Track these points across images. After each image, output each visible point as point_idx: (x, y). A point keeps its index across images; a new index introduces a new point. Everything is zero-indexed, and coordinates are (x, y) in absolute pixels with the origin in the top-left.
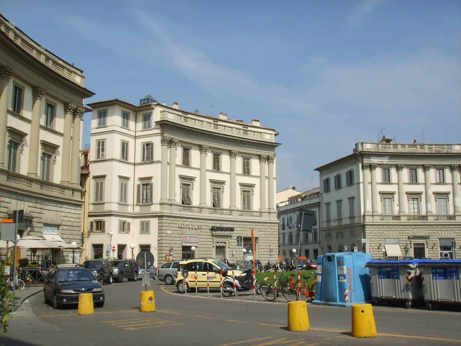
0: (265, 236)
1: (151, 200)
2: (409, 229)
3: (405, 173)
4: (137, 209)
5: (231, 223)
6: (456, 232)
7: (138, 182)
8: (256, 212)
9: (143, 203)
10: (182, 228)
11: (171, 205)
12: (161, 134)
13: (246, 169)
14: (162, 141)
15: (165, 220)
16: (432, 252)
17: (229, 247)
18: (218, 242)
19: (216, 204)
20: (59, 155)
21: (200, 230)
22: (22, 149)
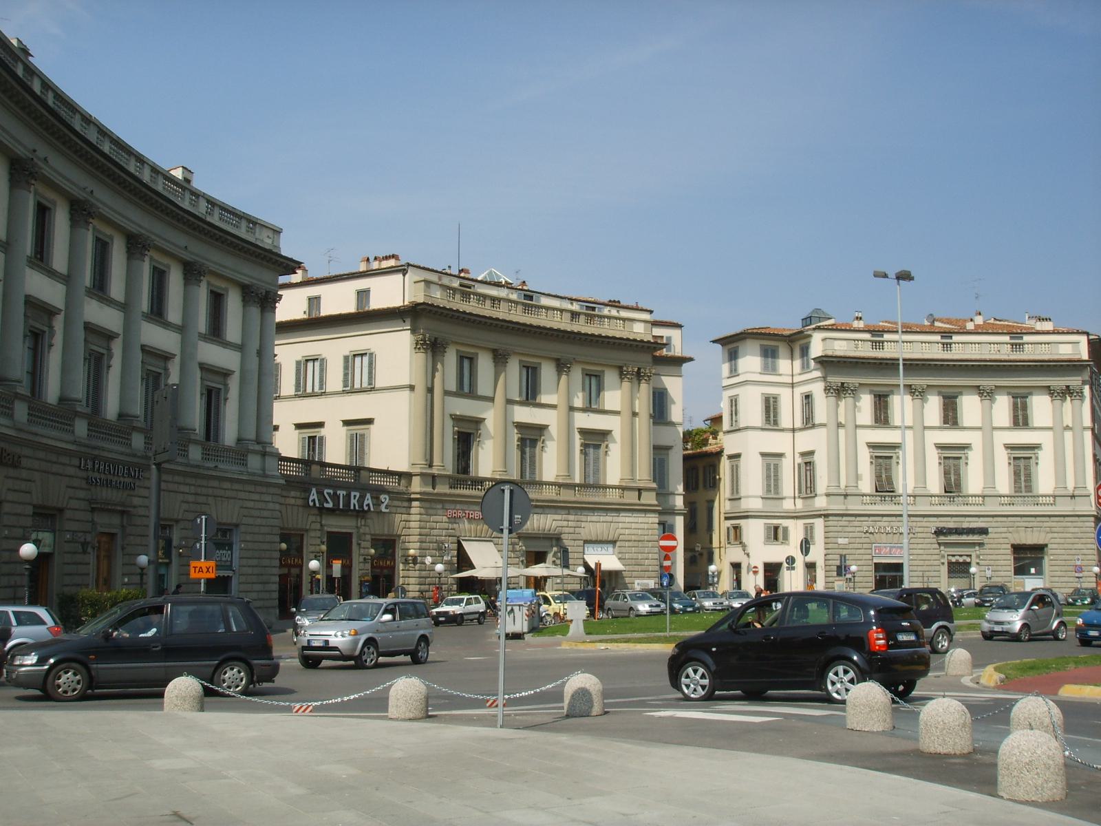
0: (1062, 541)
4: (800, 504)
5: (982, 519)
7: (799, 460)
9: (807, 493)
10: (872, 533)
12: (823, 377)
13: (1020, 417)
14: (825, 390)
18: (953, 556)
19: (953, 487)
20: (615, 442)
22: (542, 445)
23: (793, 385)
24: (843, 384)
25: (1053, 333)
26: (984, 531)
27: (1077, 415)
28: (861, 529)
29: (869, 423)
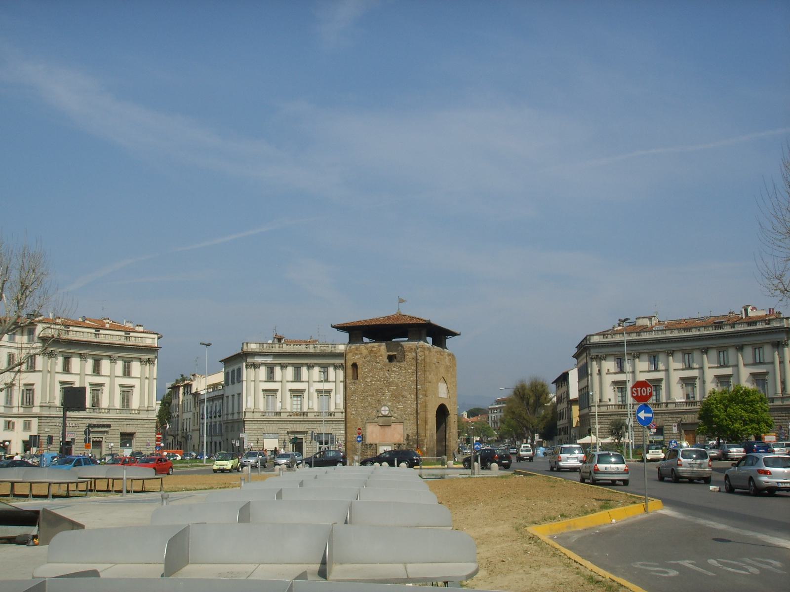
1: (33, 404)
2: (288, 425)
3: (290, 371)
4: (21, 410)
6: (334, 427)
8: (104, 409)
11: (50, 407)
13: (127, 372)
15: (43, 420)
16: (310, 446)
17: (105, 442)
18: (95, 438)
21: (77, 427)
23: (22, 349)
25: (143, 332)
26: (109, 426)
27: (151, 372)
28: (55, 424)
29: (61, 371)
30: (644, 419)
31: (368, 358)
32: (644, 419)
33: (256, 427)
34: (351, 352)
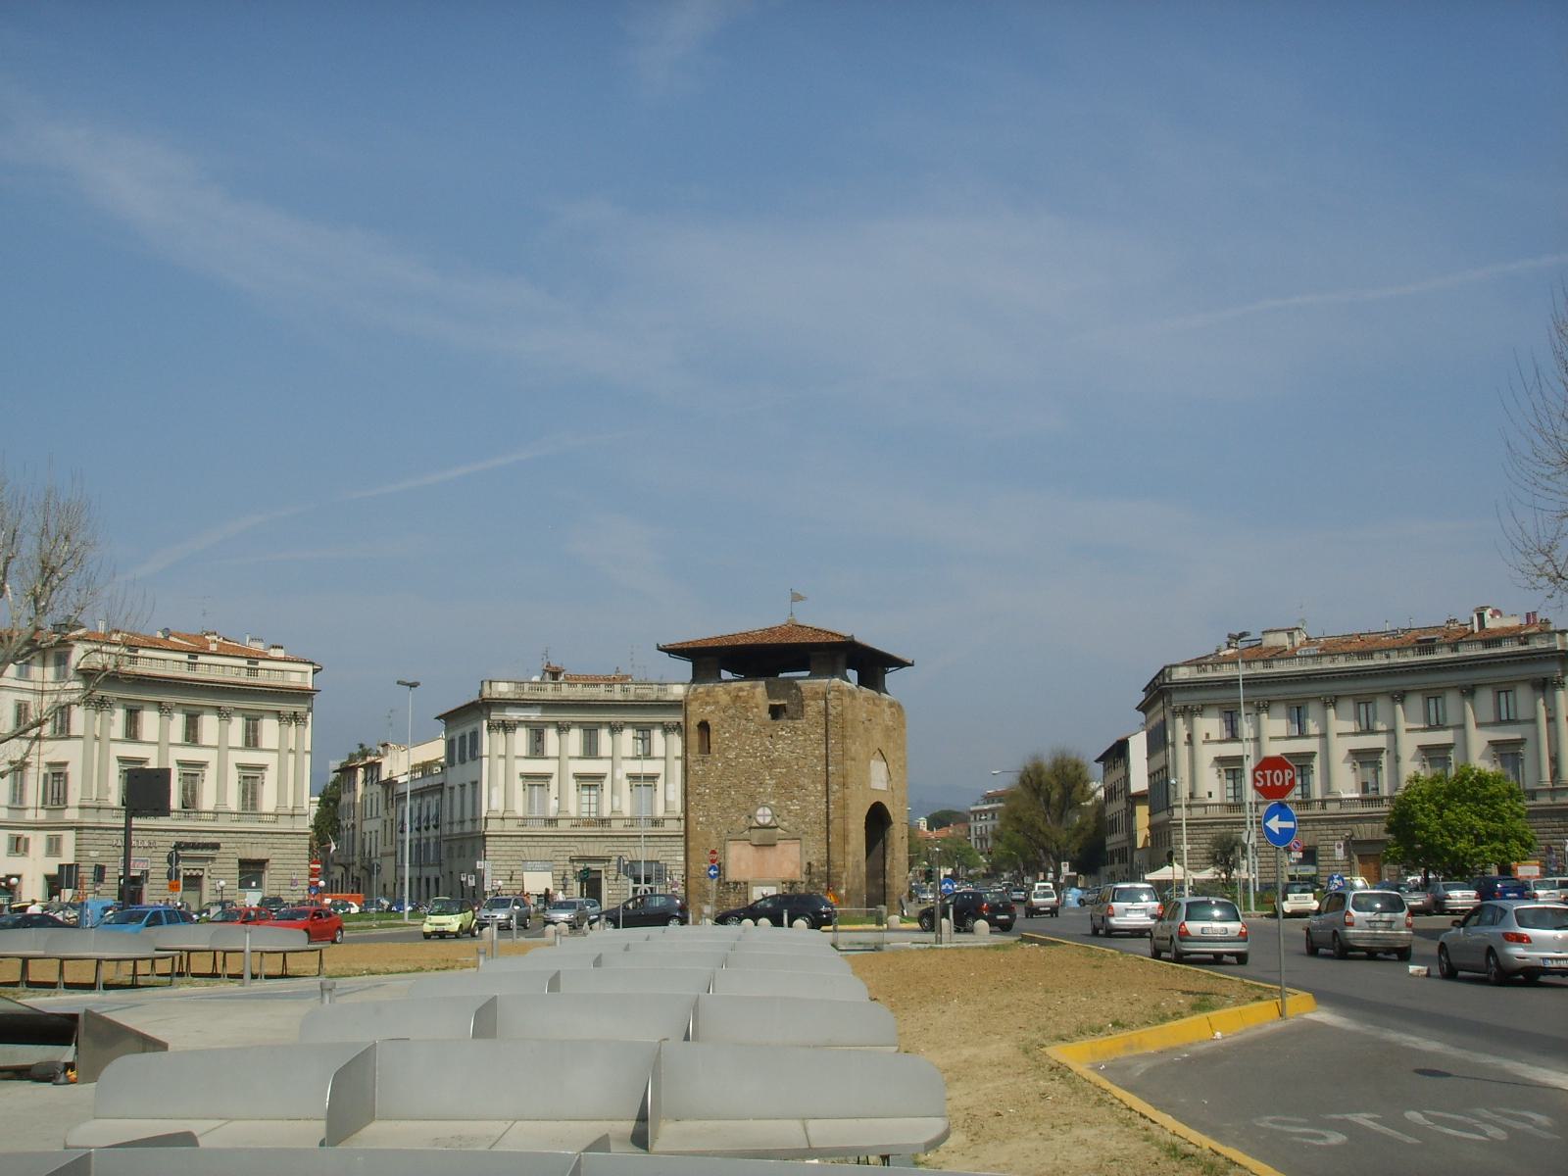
1: (65, 802)
2: (572, 844)
3: (575, 737)
4: (42, 815)
6: (662, 848)
11: (99, 808)
13: (251, 738)
15: (86, 834)
16: (615, 887)
17: (209, 877)
18: (188, 869)
21: (154, 849)
23: (43, 692)
24: (295, 713)
25: (285, 660)
26: (216, 846)
27: (299, 738)
28: (110, 842)
29: (120, 737)
30: (1277, 832)
31: (731, 712)
32: (1277, 832)
33: (508, 849)
34: (696, 699)
